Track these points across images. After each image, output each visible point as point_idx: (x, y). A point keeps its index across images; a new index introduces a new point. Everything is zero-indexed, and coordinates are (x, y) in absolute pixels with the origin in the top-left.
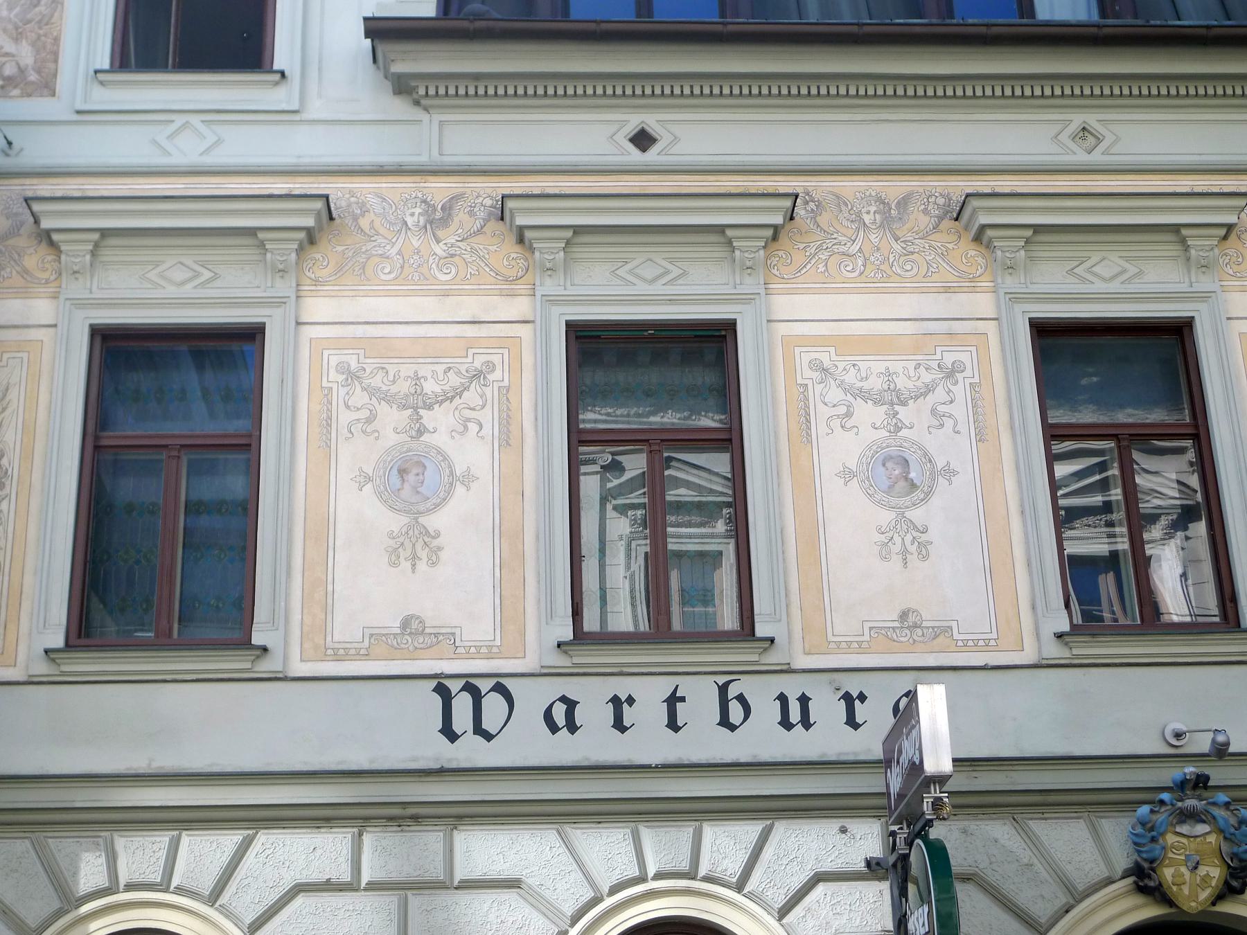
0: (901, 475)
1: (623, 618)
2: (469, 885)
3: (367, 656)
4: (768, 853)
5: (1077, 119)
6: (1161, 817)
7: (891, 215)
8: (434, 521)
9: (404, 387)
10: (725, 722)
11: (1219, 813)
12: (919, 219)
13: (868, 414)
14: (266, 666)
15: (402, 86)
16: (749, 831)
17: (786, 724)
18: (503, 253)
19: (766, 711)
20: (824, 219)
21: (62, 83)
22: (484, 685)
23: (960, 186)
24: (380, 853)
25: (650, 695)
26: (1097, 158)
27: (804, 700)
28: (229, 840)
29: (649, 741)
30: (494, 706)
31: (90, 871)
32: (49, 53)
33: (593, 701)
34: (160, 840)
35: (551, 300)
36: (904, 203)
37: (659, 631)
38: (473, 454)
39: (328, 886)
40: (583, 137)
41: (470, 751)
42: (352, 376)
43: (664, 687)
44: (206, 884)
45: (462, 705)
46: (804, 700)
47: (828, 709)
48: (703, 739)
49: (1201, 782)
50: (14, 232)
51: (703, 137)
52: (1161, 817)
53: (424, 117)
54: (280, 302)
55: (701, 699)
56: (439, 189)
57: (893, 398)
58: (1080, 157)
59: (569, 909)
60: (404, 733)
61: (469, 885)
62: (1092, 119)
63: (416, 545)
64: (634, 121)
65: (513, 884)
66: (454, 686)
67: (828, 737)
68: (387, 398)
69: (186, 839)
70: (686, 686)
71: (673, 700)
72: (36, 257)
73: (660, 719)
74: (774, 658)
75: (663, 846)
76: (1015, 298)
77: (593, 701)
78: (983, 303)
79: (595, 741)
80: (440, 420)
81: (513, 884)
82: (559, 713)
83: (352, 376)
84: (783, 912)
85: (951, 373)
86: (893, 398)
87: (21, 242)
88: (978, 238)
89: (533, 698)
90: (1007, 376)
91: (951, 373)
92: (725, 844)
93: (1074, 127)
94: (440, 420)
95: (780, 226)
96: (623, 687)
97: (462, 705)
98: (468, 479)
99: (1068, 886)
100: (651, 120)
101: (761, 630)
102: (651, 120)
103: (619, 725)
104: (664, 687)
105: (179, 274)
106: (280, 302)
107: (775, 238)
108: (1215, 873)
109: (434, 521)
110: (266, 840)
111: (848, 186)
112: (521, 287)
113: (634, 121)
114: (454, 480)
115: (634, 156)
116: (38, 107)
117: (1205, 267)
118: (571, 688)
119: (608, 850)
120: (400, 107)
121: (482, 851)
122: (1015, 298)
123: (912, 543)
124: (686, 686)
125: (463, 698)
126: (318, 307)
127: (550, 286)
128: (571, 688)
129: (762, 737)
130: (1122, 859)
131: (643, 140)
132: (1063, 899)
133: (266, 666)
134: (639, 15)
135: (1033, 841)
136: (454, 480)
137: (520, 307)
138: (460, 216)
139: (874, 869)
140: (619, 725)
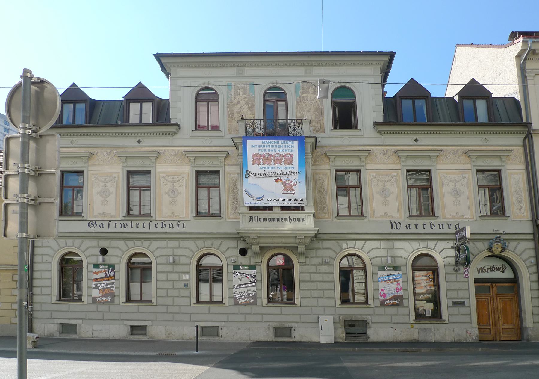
0: (456, 193)
1: (414, 213)
2: (396, 249)
3: (380, 218)
4: (437, 245)
5: (485, 137)
6: (493, 242)
7: (455, 153)
8: (388, 199)
9: (103, 180)
10: (431, 228)
11: (502, 242)
12: (112, 154)
13: (452, 184)
14: (366, 219)
15: (379, 132)
16: (435, 242)
17: (440, 228)
18: (395, 159)
19: (437, 226)
20: (444, 153)
21: (326, 131)
22: (397, 222)
23: (183, 149)
24: (384, 244)
25: (420, 224)
26: (487, 143)
27: (442, 225)
28: (363, 242)
29: (420, 230)
30: (398, 225)
31: (344, 246)
32: (323, 126)
33: (412, 225)
34: (354, 242)
35: (404, 166)
36: (457, 151)
37: (421, 216)
38: (113, 190)
39: (377, 248)
40: (408, 140)
41: (395, 231)
42: (374, 178)
43: (423, 223)
44: (360, 248)
45: (394, 225)
46: (442, 225)
47: (446, 226)
48: (428, 230)
49: (500, 237)
50: (322, 155)
51: (425, 140)
52: (493, 242)
53: (381, 136)
54: (222, 167)
55: (428, 224)
56: (386, 148)
57: (455, 182)
58: (485, 144)
59: (410, 252)
60: (387, 229)
61: (396, 249)
62: (487, 137)
63: (386, 202)
64: (415, 137)
65: (402, 249)
66: (393, 222)
67: (446, 230)
68: (450, 181)
69: (357, 242)
70: (146, 222)
71: (424, 225)
72: (326, 159)
73: (422, 226)
74: (438, 219)
75: (423, 244)
76: (474, 166)
77: (412, 225)
78: (469, 167)
79: (413, 230)
80: (388, 184)
81: (402, 249)
82: (408, 226)
83: (374, 178)
84: (439, 253)
85: (464, 178)
86: (455, 182)
87: (323, 157)
88: (469, 157)
89: (404, 224)
90: (401, 178)
91: (464, 178)
92: (431, 244)
93: (414, 139)
94: (108, 184)
95: (436, 154)
96: (417, 223)
97: (394, 225)
98: (112, 193)
99: (479, 250)
100: (140, 138)
101: (436, 215)
102: (140, 138)
103: (416, 228)
104: (423, 223)
105: (207, 163)
106: (222, 167)
107: (89, 158)
108: (500, 249)
109: (388, 199)
110: (368, 242)
111: (449, 148)
112: (399, 164)
113: (415, 137)
114: (178, 193)
115: (138, 144)
116: (322, 135)
117: (503, 161)
118: (409, 223)
119: (415, 245)
120: (378, 135)
121: (398, 244)
122: (474, 166)
123: (386, 202)
124: (146, 222)
125: (394, 224)
126: (368, 167)
127: (403, 164)
128: (409, 223)
129: (436, 230)
130: (487, 247)
131: (416, 140)
132: (478, 252)
133: (366, 219)
134: (86, 123)
135: (474, 244)
136: (178, 193)
137: (399, 167)
138: (389, 153)
139: (452, 248)
140: (416, 228)
